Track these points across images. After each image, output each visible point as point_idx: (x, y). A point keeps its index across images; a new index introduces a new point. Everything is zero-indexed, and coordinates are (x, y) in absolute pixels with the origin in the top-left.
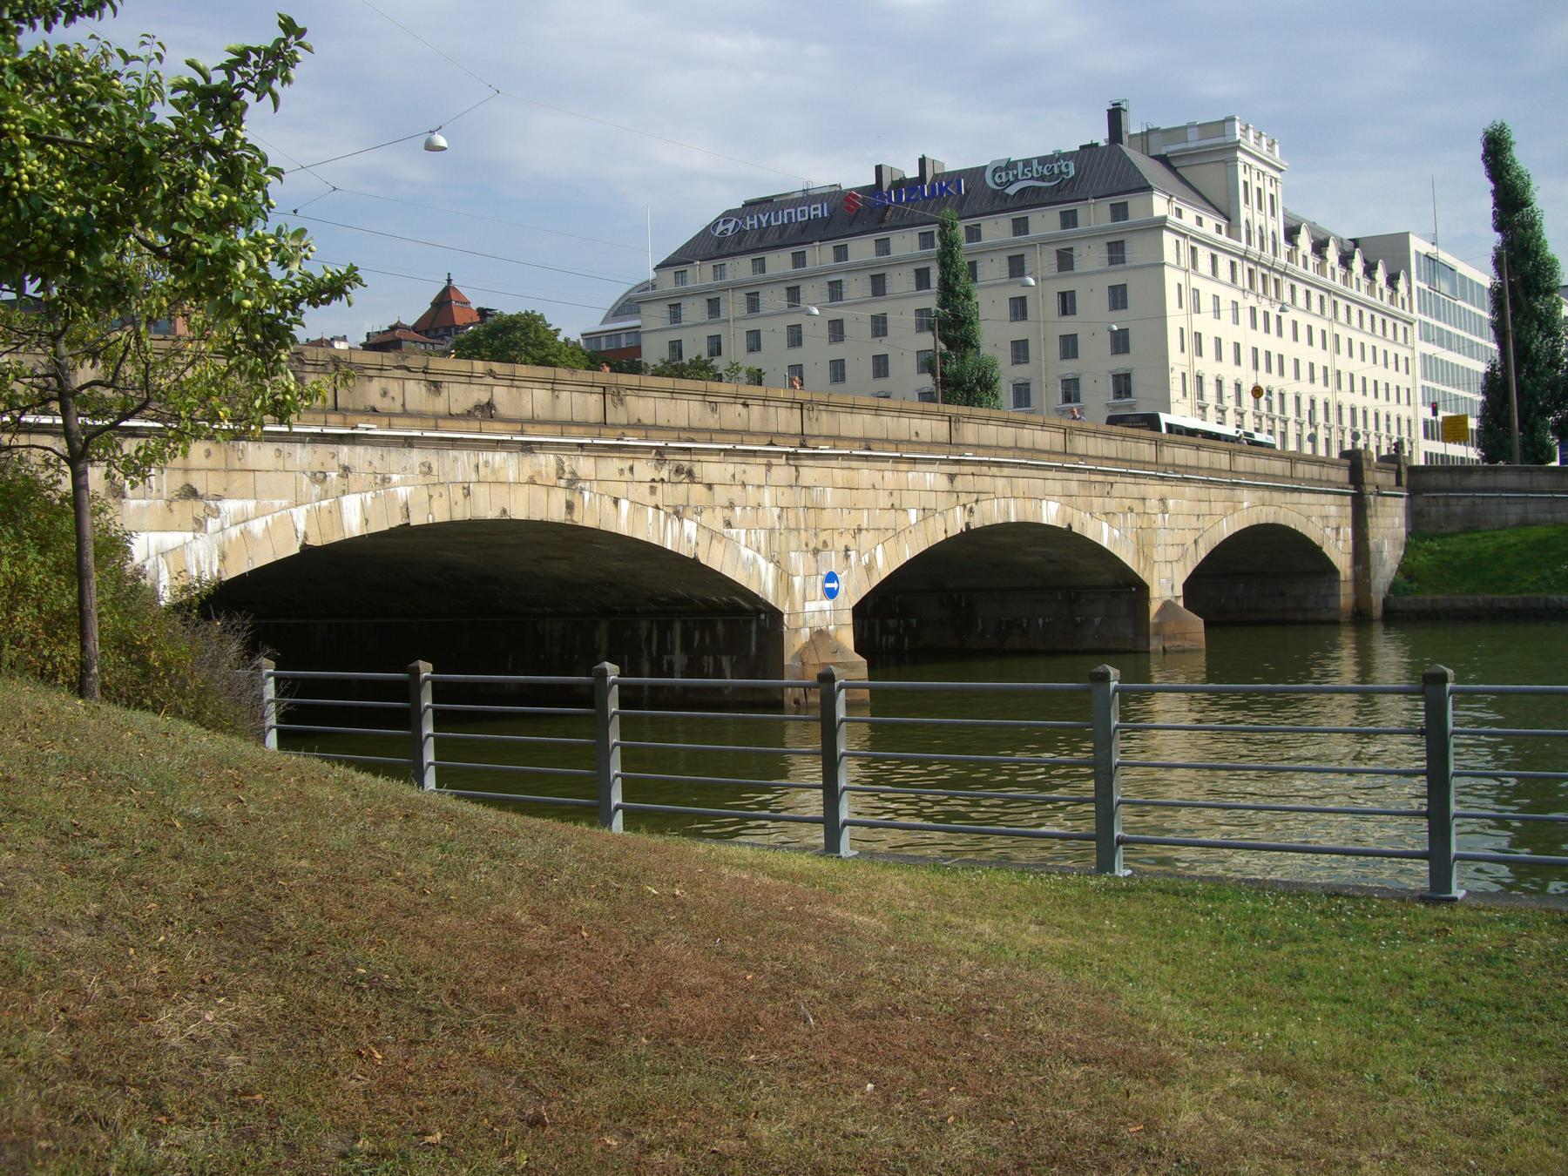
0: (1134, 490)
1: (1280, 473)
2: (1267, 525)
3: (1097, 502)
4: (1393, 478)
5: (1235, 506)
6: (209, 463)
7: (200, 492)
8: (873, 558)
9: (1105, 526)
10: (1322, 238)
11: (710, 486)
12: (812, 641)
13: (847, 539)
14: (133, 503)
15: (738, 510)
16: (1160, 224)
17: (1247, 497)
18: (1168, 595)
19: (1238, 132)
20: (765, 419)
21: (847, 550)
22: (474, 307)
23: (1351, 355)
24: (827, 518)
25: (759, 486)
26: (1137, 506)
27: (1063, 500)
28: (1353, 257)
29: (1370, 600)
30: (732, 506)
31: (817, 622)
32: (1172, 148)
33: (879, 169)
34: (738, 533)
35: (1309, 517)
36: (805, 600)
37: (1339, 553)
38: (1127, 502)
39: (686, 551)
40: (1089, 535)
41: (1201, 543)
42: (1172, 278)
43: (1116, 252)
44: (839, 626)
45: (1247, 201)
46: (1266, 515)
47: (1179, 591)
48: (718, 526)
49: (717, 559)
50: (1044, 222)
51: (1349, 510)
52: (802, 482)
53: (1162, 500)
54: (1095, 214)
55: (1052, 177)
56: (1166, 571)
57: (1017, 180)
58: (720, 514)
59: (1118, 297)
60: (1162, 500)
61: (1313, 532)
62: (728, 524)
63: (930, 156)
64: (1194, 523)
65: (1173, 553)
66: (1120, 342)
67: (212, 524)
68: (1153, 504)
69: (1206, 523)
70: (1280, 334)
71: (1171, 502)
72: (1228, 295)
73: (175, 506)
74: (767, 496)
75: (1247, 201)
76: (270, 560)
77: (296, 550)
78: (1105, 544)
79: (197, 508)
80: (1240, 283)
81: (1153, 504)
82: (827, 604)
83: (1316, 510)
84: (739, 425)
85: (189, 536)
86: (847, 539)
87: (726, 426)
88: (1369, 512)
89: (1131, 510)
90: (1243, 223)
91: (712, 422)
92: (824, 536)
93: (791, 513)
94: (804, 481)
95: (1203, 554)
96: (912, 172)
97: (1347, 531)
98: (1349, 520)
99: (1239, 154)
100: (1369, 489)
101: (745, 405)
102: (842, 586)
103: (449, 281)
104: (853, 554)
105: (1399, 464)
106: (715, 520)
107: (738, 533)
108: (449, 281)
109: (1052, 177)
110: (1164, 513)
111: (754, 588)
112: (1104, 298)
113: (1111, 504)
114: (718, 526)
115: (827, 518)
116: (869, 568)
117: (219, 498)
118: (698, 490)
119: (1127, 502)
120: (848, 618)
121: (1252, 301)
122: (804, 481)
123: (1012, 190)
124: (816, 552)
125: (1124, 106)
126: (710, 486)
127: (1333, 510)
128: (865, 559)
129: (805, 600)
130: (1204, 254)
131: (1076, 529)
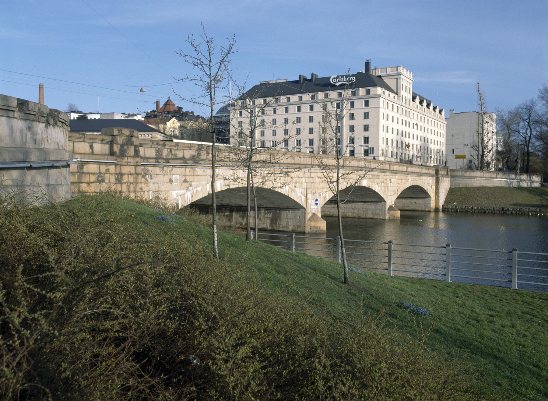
0: (384, 177)
1: (418, 172)
2: (415, 185)
3: (376, 180)
4: (446, 173)
5: (407, 180)
6: (190, 174)
7: (188, 181)
8: (326, 196)
9: (377, 186)
10: (422, 99)
11: (292, 178)
12: (312, 216)
13: (320, 191)
14: (175, 183)
15: (298, 183)
16: (379, 96)
17: (410, 178)
18: (391, 204)
19: (401, 70)
20: (304, 161)
21: (320, 193)
22: (176, 106)
23: (431, 134)
24: (316, 185)
25: (302, 178)
26: (385, 181)
27: (368, 180)
28: (423, 102)
29: (439, 205)
30: (296, 183)
31: (314, 211)
32: (383, 74)
33: (300, 76)
34: (298, 189)
35: (425, 183)
36: (311, 206)
37: (432, 192)
38: (382, 180)
39: (286, 194)
40: (373, 189)
41: (399, 190)
42: (382, 111)
43: (367, 104)
44: (318, 212)
45: (402, 90)
46: (415, 183)
47: (393, 203)
48: (293, 188)
49: (293, 196)
50: (347, 93)
51: (435, 181)
52: (311, 176)
53: (390, 180)
54: (362, 92)
55: (349, 81)
56: (390, 197)
57: (339, 81)
58: (294, 184)
59: (366, 116)
60: (390, 180)
61: (425, 187)
62: (295, 187)
63: (314, 73)
64: (397, 185)
65: (392, 193)
66: (366, 128)
67: (190, 188)
68: (388, 180)
69: (400, 185)
70: (409, 126)
71: (392, 180)
72: (396, 116)
73: (183, 184)
74: (304, 180)
75: (402, 90)
76: (202, 197)
77: (207, 195)
78: (377, 191)
79: (187, 185)
80: (399, 113)
81: (388, 180)
82: (316, 207)
83: (426, 181)
84: (298, 162)
85: (186, 191)
86: (320, 191)
87: (296, 163)
88: (440, 182)
89: (383, 182)
90: (401, 96)
91: (292, 162)
92: (315, 190)
93: (309, 184)
94: (312, 176)
95: (399, 194)
96: (309, 77)
97: (434, 187)
98: (435, 184)
99: (401, 76)
100: (440, 176)
101: (300, 157)
102: (319, 202)
103: (169, 98)
104: (321, 194)
105: (448, 169)
106: (292, 186)
107: (298, 189)
108: (169, 98)
109: (349, 81)
110: (391, 182)
111: (300, 203)
112: (363, 116)
113: (379, 181)
114: (293, 188)
115: (316, 185)
116: (325, 198)
117: (192, 182)
118: (289, 179)
119: (382, 180)
120: (320, 210)
121: (402, 117)
122: (312, 176)
123: (337, 84)
124: (314, 194)
125: (370, 61)
126: (292, 178)
127: (430, 181)
128: (324, 195)
129: (311, 206)
130: (390, 104)
131: (370, 187)
